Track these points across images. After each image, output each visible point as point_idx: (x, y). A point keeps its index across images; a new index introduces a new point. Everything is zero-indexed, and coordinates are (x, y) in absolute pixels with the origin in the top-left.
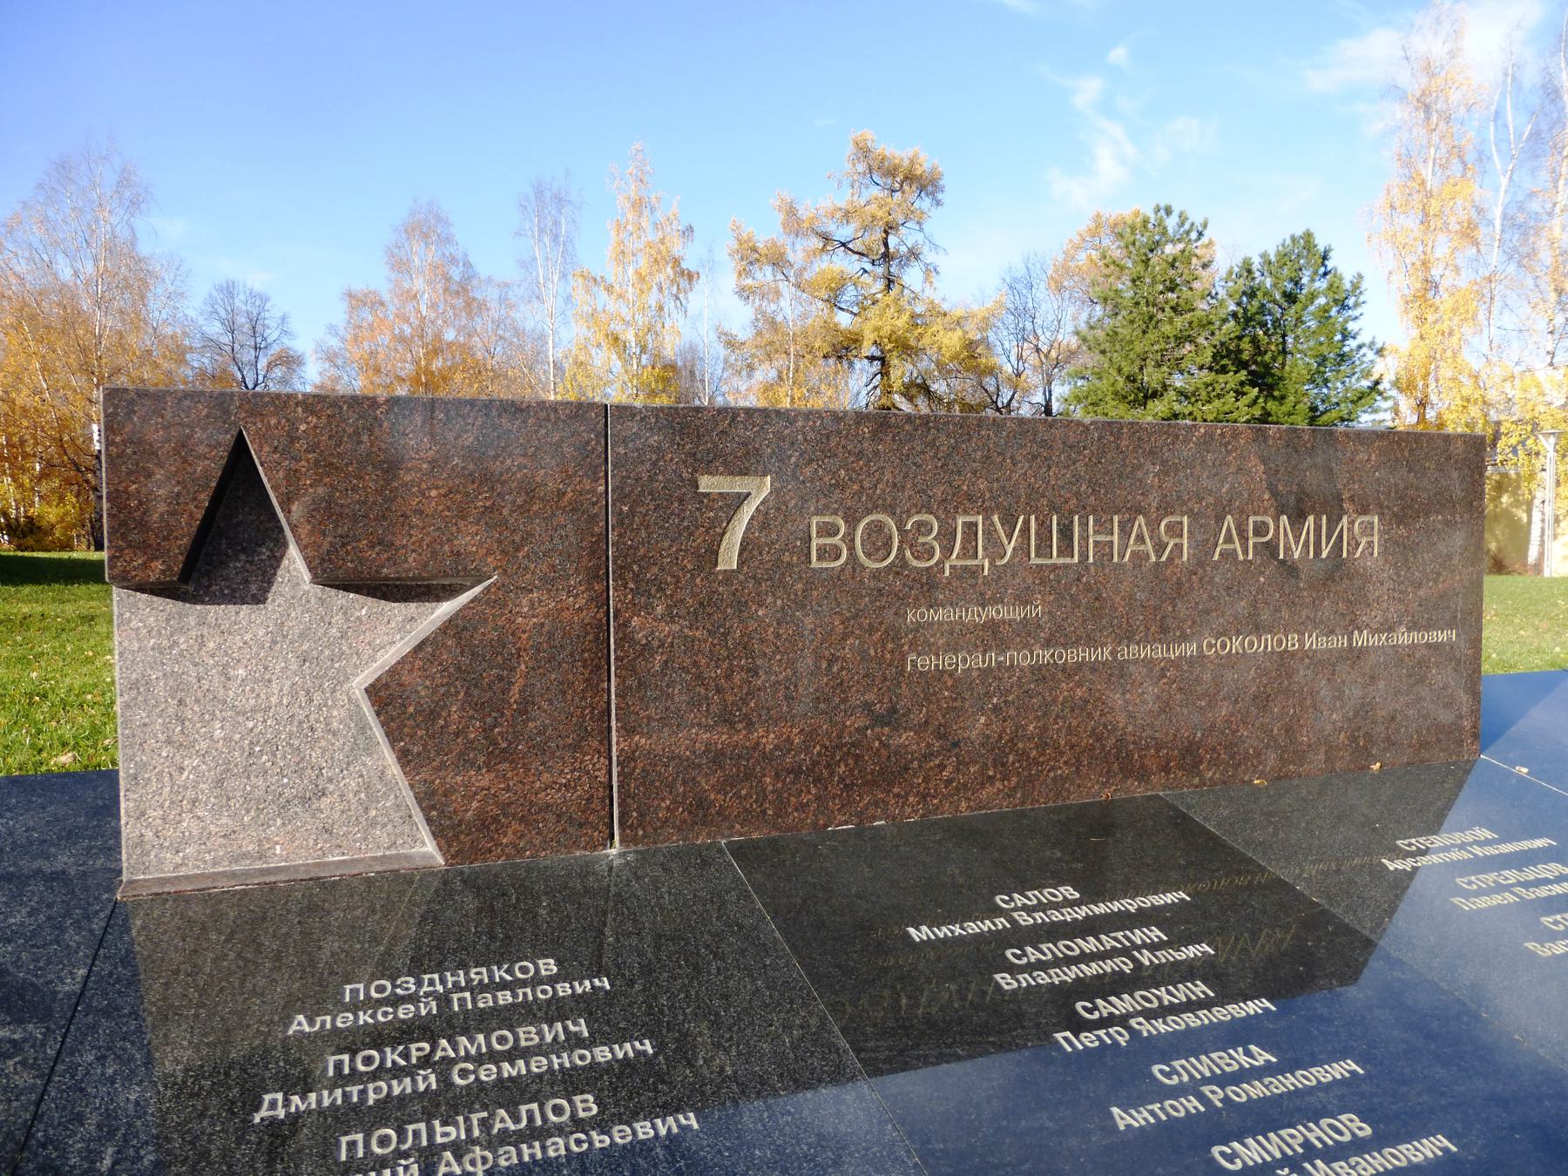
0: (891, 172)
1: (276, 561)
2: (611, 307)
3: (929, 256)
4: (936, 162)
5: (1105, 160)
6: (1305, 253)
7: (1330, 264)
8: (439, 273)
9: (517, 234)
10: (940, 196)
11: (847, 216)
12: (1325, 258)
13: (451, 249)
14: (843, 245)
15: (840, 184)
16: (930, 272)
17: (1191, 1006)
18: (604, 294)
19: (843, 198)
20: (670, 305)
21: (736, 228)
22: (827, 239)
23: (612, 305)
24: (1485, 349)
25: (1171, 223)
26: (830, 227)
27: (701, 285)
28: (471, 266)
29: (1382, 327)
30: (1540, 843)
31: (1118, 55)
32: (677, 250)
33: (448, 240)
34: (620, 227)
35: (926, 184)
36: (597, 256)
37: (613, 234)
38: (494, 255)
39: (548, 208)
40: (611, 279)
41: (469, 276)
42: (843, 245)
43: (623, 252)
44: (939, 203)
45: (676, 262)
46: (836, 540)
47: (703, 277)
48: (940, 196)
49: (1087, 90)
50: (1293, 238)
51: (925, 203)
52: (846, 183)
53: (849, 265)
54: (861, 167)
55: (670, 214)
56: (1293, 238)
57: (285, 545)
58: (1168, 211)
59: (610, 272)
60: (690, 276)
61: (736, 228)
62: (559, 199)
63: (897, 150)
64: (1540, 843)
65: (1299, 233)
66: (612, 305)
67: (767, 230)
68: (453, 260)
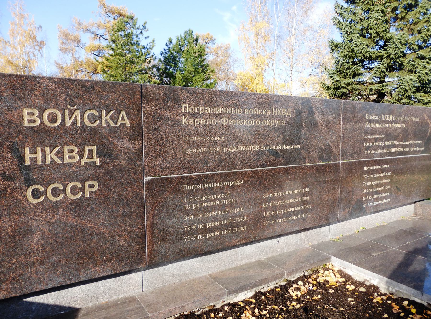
15: (96, 15)
19: (98, 20)
20: (36, 52)
22: (95, 34)
26: (94, 29)
42: (101, 36)
53: (104, 43)
59: (11, 40)
60: (42, 43)
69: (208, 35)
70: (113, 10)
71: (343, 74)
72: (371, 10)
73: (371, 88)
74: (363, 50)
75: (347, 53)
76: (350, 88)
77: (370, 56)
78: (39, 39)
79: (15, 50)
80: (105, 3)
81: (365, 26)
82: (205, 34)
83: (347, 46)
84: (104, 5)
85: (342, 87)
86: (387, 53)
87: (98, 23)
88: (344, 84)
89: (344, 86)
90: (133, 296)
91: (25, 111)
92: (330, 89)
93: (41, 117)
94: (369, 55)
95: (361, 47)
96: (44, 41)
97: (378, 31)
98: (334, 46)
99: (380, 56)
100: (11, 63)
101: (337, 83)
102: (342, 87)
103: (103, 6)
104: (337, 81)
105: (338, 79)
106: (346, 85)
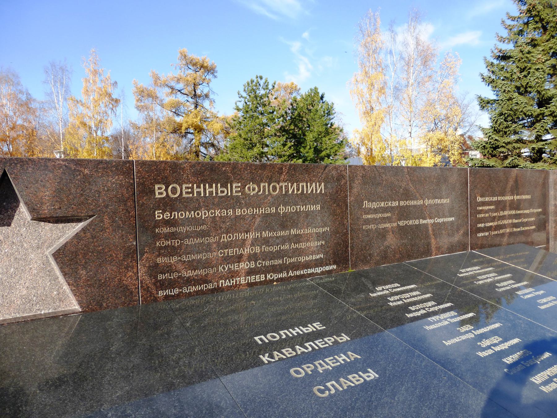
0: (195, 65)
1: (18, 206)
2: (84, 112)
3: (211, 96)
4: (213, 61)
5: (302, 69)
6: (315, 98)
7: (324, 99)
8: (13, 97)
9: (45, 82)
10: (216, 74)
11: (178, 80)
12: (322, 98)
13: (19, 88)
14: (179, 91)
15: (176, 68)
16: (212, 102)
17: (416, 296)
18: (81, 107)
19: (178, 73)
20: (109, 112)
21: (135, 83)
22: (172, 88)
23: (85, 111)
24: (390, 131)
25: (262, 82)
26: (173, 84)
27: (121, 106)
28: (30, 94)
29: (350, 123)
30: (412, 286)
31: (306, 35)
32: (110, 90)
33: (18, 84)
34: (87, 81)
35: (209, 70)
36: (78, 93)
37: (84, 84)
38: (37, 89)
39: (59, 74)
40: (84, 101)
41: (30, 99)
42: (179, 91)
43: (87, 90)
44: (215, 77)
45: (110, 95)
46: (278, 186)
47: (122, 101)
48: (216, 74)
49: (296, 46)
50: (311, 90)
51: (210, 76)
52: (178, 68)
53: (181, 98)
54: (184, 62)
55: (107, 77)
56: (311, 90)
57: (17, 201)
58: (261, 78)
59: (83, 98)
60: (117, 101)
61: (135, 83)
62: (63, 70)
63: (198, 57)
64: (412, 286)
65: (313, 88)
66: (85, 111)
67: (147, 83)
68: (21, 92)
69: (293, 84)
70: (194, 62)
71: (501, 133)
72: (528, 68)
73: (534, 146)
74: (525, 109)
75: (506, 112)
76: (510, 147)
77: (532, 115)
78: (114, 97)
79: (87, 110)
80: (186, 54)
81: (524, 84)
82: (289, 83)
83: (506, 105)
84: (185, 56)
85: (503, 146)
86: (551, 111)
87: (179, 77)
88: (504, 143)
89: (504, 145)
90: (20, 392)
91: (157, 187)
92: (487, 148)
93: (166, 190)
94: (530, 114)
95: (523, 105)
96: (121, 99)
97: (539, 89)
98: (484, 104)
99: (541, 114)
100: (85, 124)
101: (496, 142)
102: (503, 146)
103: (183, 58)
104: (496, 140)
105: (497, 138)
106: (505, 143)
